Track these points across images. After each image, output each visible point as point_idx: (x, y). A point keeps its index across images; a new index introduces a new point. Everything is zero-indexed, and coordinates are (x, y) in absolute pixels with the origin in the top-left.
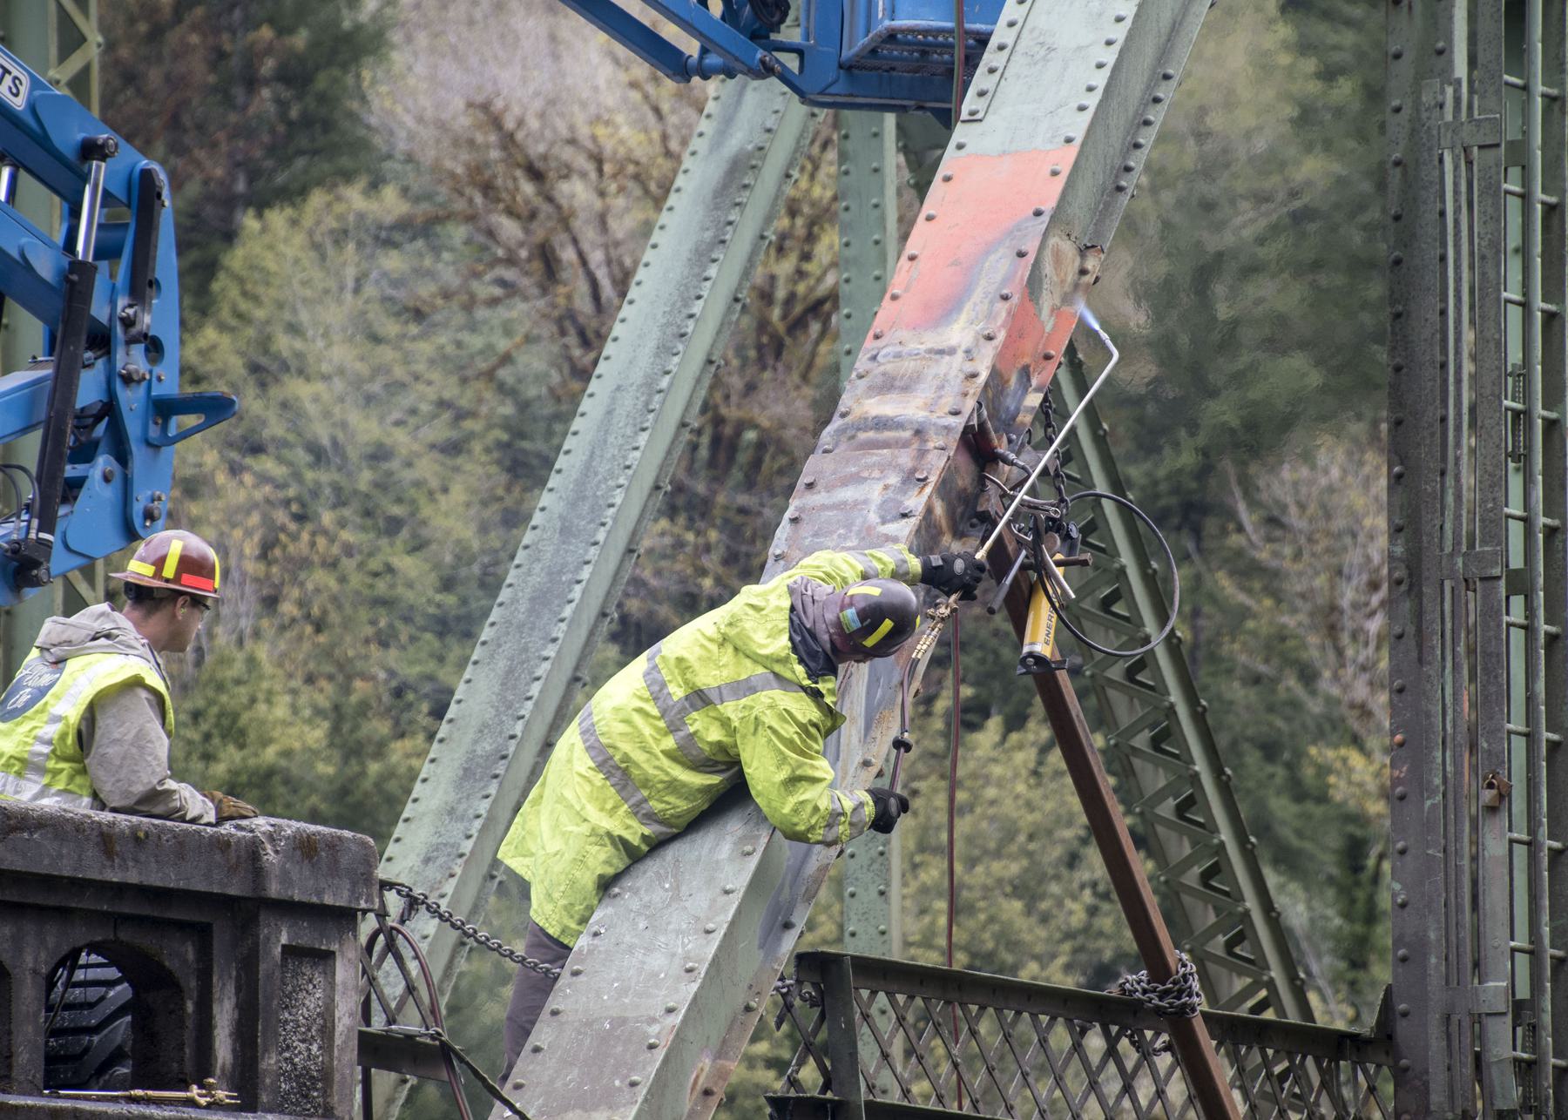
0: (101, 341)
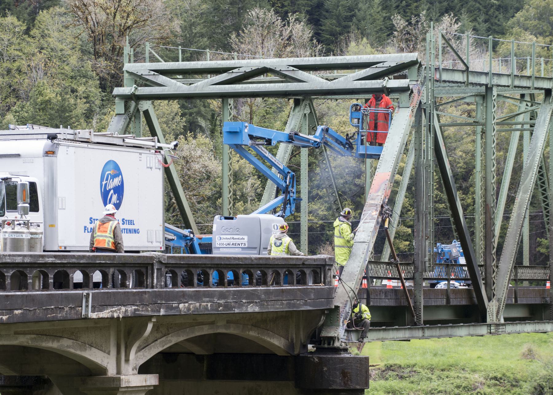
0: (289, 193)
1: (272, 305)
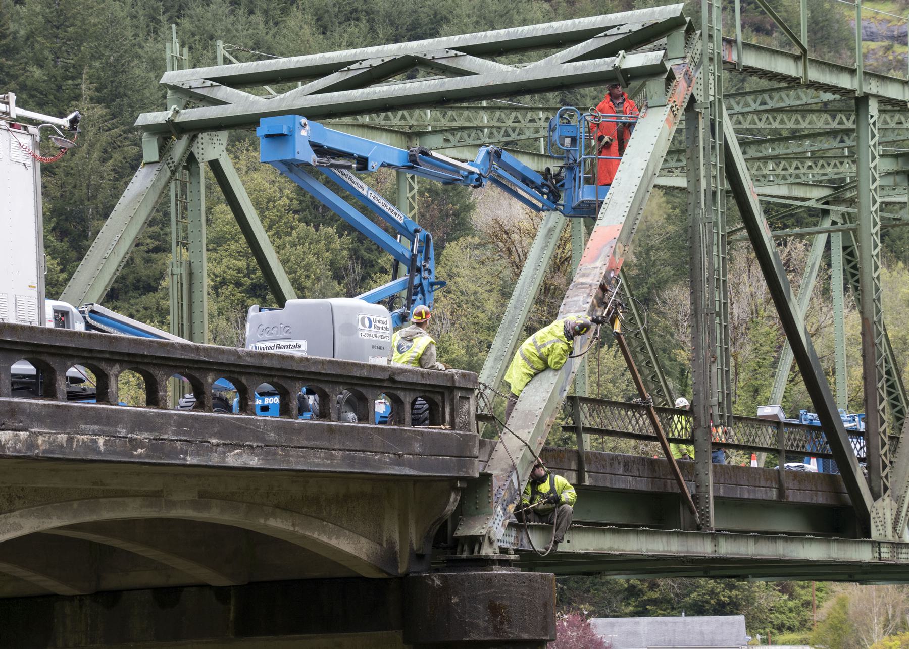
1: (298, 456)
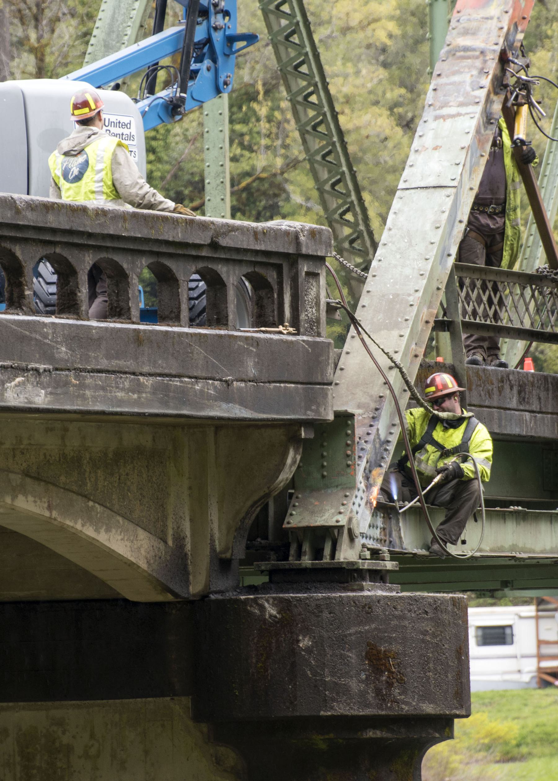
1: (97, 388)
